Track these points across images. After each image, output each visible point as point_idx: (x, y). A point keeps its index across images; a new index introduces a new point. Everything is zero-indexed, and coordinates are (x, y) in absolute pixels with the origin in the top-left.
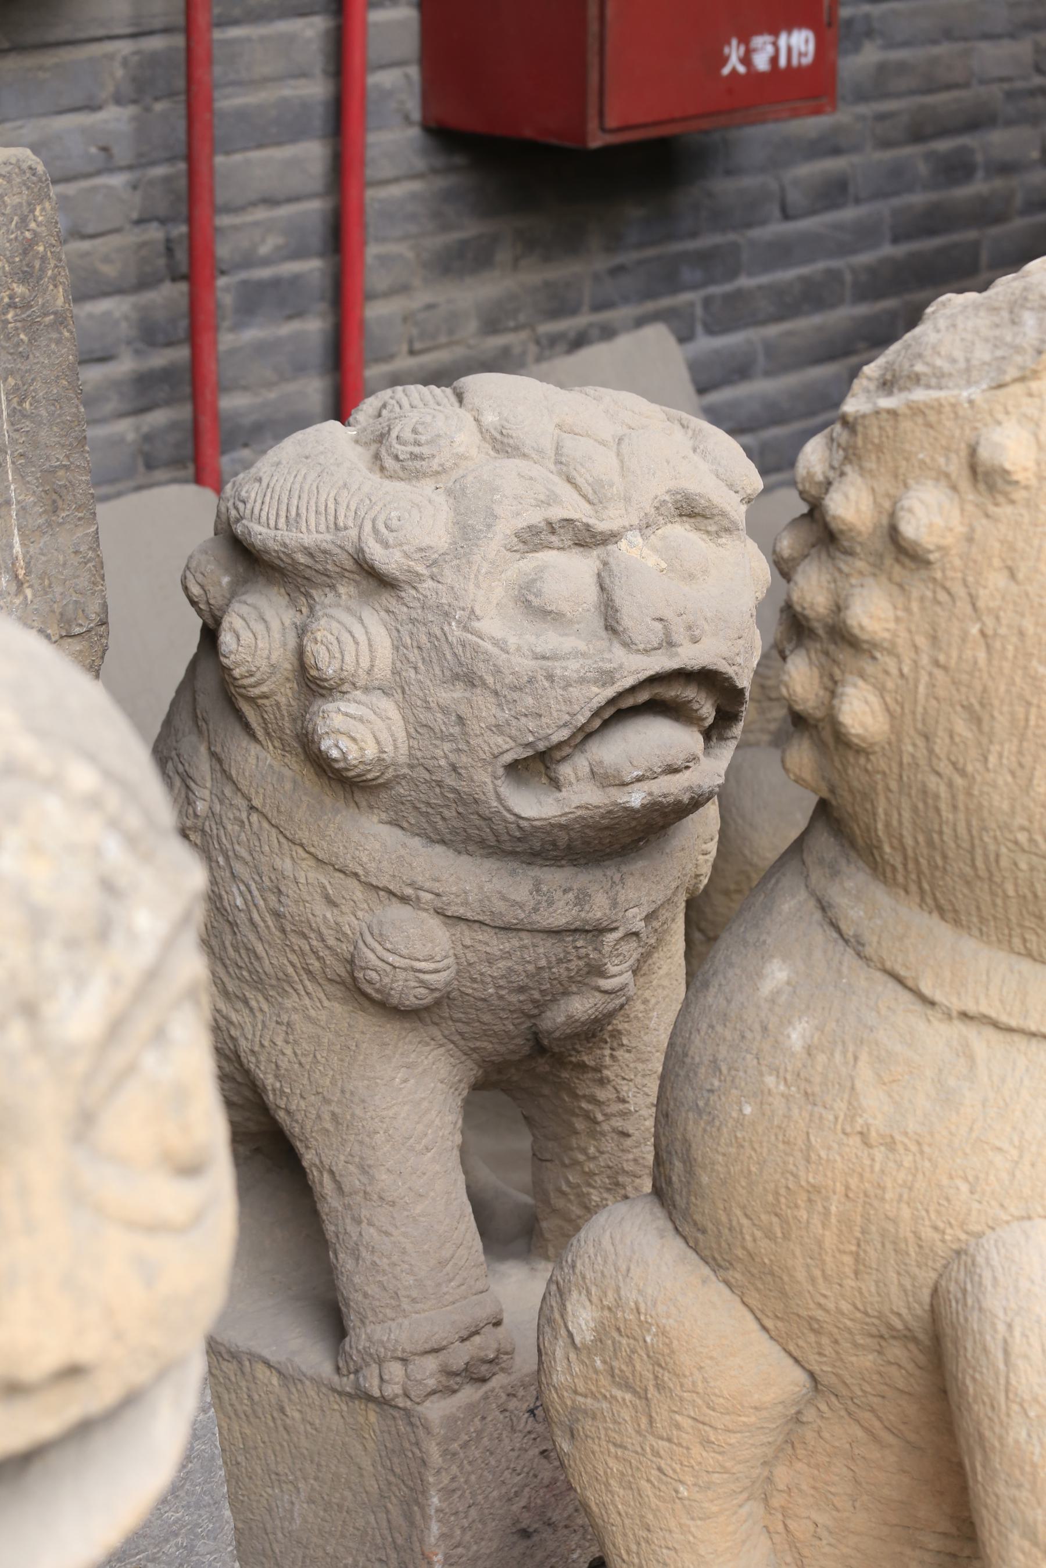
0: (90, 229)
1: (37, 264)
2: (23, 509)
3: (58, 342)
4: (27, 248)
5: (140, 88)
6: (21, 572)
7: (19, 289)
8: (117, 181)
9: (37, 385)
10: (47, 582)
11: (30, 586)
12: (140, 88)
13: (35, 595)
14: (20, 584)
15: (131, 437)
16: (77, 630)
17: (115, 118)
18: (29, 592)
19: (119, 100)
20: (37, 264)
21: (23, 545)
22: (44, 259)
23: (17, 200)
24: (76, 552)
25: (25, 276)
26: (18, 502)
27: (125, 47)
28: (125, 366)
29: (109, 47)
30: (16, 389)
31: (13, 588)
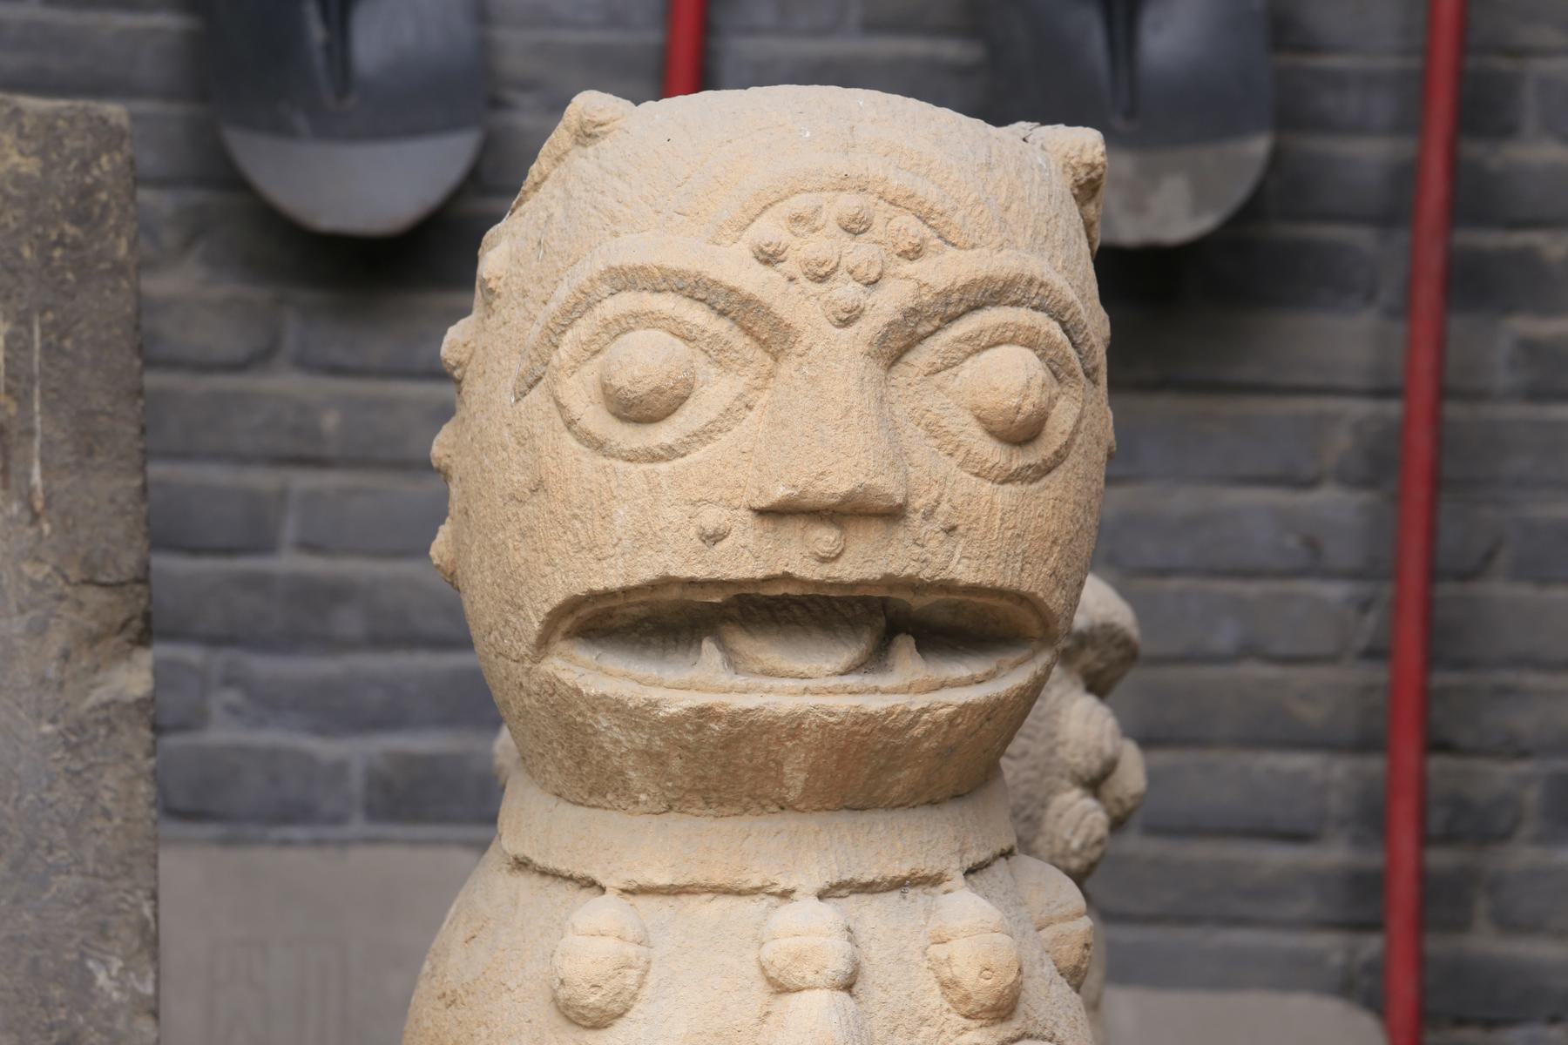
0: (1281, 648)
1: (97, 210)
2: (48, 444)
3: (114, 290)
4: (86, 193)
5: (1377, 465)
6: (39, 505)
7: (71, 230)
8: (1335, 592)
9: (82, 326)
10: (70, 522)
11: (50, 521)
12: (1377, 465)
13: (53, 530)
14: (35, 518)
15: (1337, 959)
16: (104, 579)
17: (1334, 504)
18: (46, 528)
19: (1344, 478)
20: (97, 210)
21: (43, 476)
22: (105, 206)
23: (78, 144)
24: (112, 501)
25: (80, 219)
26: (44, 435)
27: (1361, 408)
28: (1334, 854)
29: (1331, 405)
30: (54, 325)
31: (27, 517)
